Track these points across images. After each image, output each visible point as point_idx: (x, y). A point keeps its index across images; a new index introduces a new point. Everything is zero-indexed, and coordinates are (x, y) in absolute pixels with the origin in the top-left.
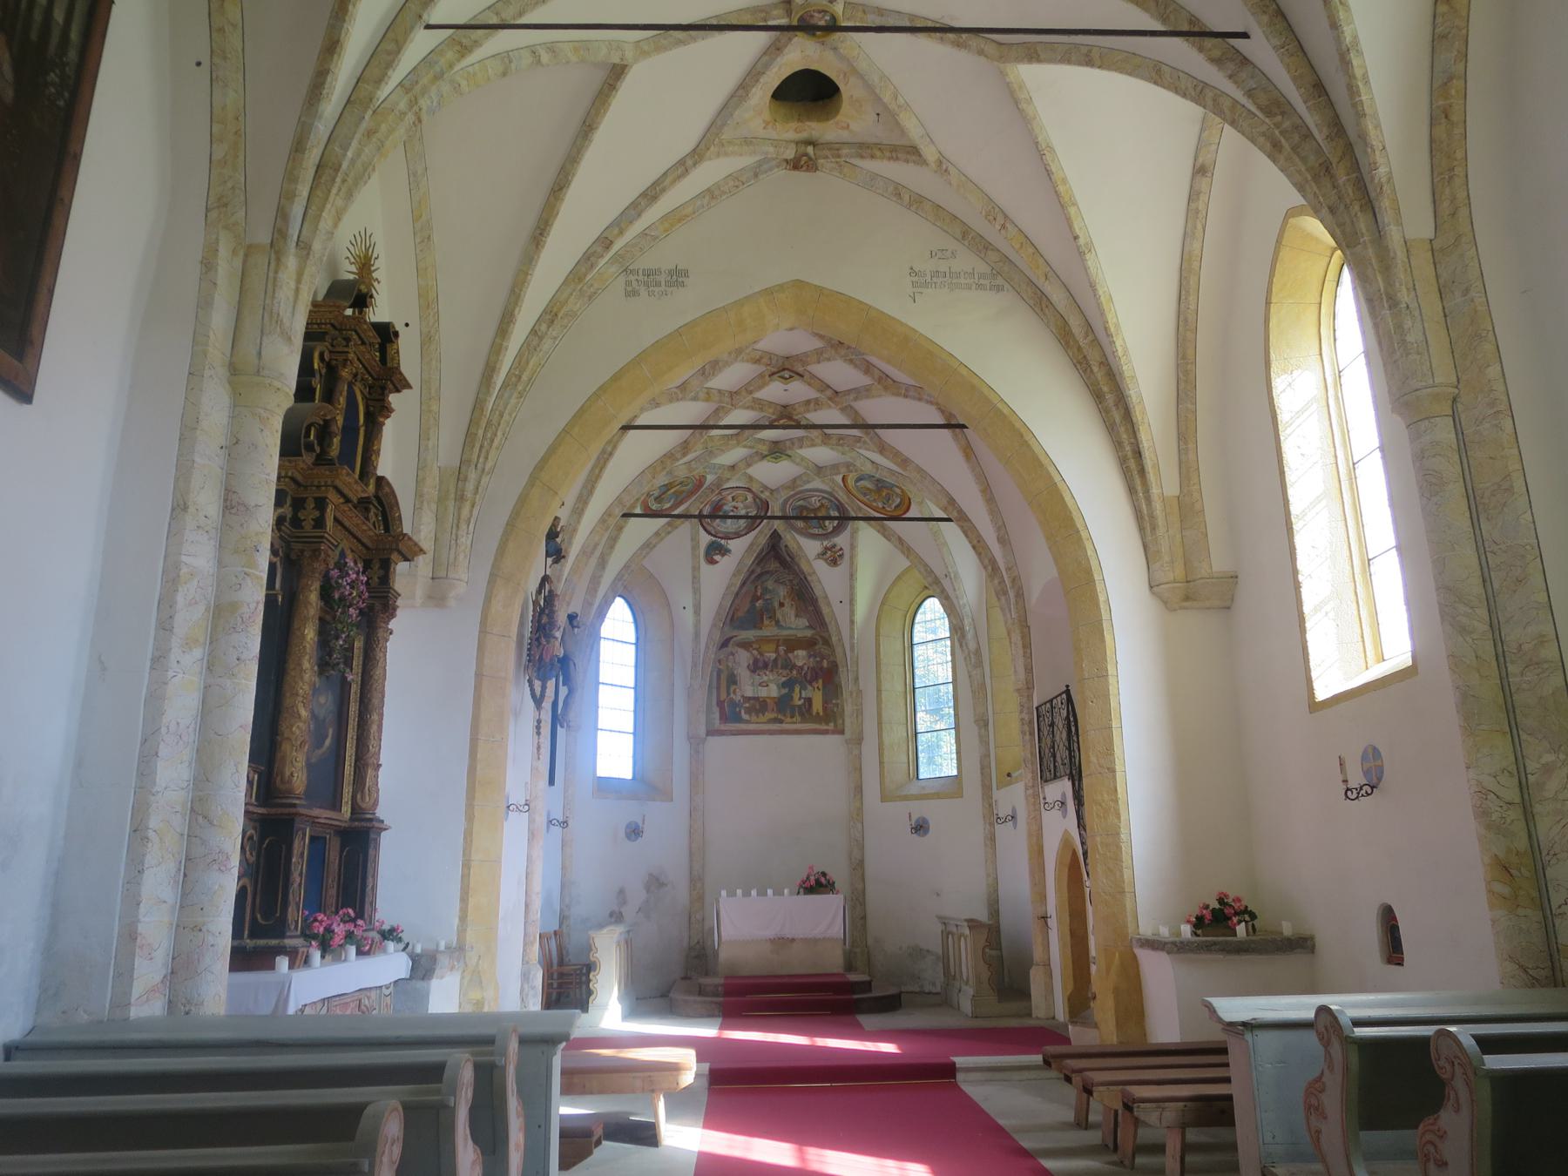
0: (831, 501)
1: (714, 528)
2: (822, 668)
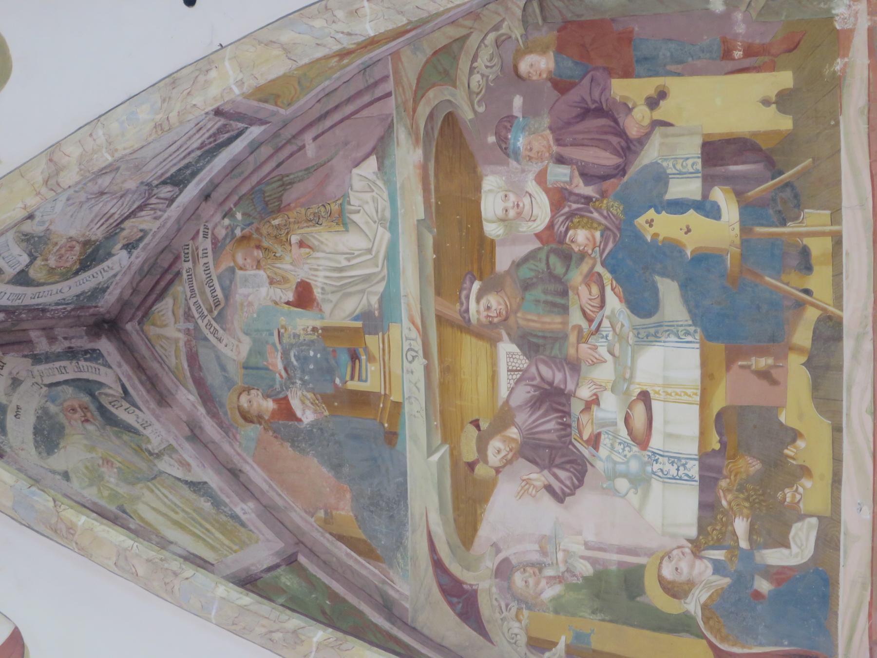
2: (561, 85)
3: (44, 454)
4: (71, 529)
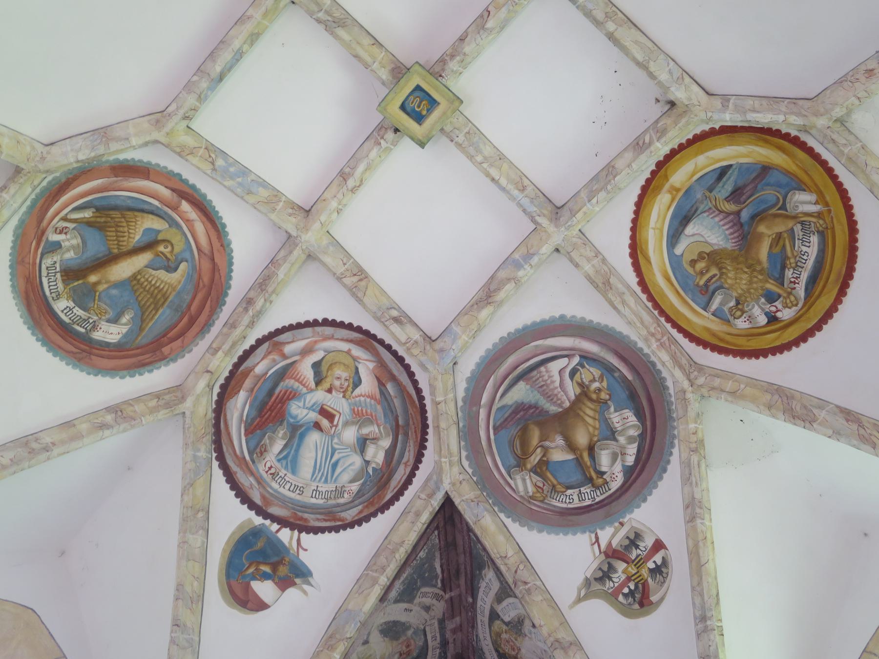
0: (609, 369)
1: (260, 481)
3: (380, 628)
4: (332, 648)
